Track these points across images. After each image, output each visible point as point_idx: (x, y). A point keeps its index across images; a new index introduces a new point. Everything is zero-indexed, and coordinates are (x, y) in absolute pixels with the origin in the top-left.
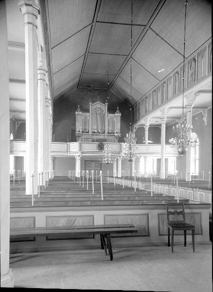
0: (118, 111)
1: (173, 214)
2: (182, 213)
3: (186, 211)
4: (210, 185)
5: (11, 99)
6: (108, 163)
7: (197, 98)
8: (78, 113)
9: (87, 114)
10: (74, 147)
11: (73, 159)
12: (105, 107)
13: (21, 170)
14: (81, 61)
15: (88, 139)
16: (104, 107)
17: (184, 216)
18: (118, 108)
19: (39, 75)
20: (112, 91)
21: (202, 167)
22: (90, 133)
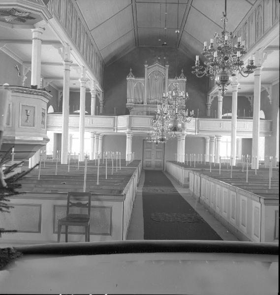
0: (182, 74)
1: (73, 205)
2: (89, 206)
3: (93, 203)
4: (272, 186)
5: (43, 63)
6: (157, 143)
7: (75, 62)
8: (130, 78)
9: (141, 79)
10: (122, 121)
11: (124, 137)
12: (165, 71)
13: (14, 145)
14: (128, 11)
15: (142, 112)
16: (163, 70)
17: (89, 211)
18: (182, 71)
19: (34, 34)
20: (181, 49)
21: (18, 140)
22: (145, 104)
